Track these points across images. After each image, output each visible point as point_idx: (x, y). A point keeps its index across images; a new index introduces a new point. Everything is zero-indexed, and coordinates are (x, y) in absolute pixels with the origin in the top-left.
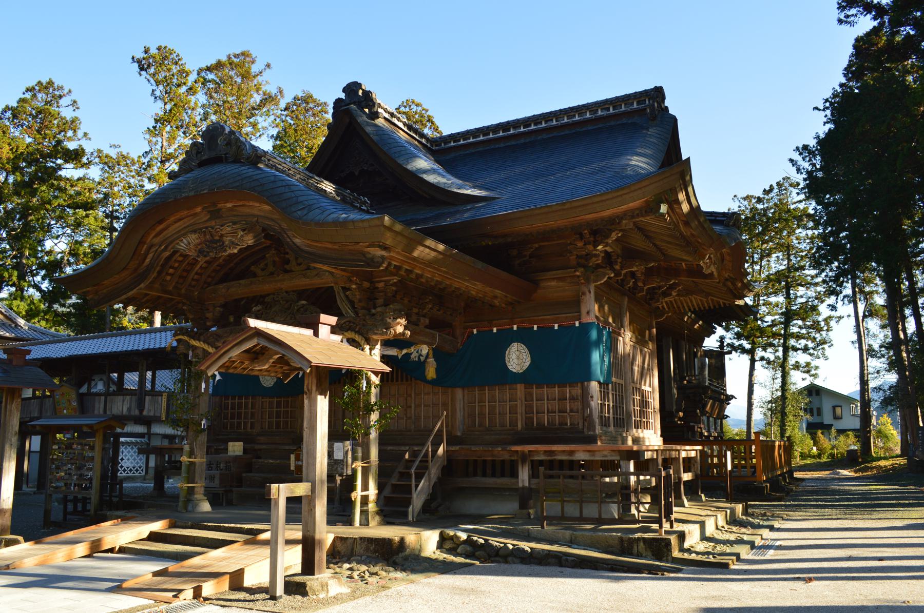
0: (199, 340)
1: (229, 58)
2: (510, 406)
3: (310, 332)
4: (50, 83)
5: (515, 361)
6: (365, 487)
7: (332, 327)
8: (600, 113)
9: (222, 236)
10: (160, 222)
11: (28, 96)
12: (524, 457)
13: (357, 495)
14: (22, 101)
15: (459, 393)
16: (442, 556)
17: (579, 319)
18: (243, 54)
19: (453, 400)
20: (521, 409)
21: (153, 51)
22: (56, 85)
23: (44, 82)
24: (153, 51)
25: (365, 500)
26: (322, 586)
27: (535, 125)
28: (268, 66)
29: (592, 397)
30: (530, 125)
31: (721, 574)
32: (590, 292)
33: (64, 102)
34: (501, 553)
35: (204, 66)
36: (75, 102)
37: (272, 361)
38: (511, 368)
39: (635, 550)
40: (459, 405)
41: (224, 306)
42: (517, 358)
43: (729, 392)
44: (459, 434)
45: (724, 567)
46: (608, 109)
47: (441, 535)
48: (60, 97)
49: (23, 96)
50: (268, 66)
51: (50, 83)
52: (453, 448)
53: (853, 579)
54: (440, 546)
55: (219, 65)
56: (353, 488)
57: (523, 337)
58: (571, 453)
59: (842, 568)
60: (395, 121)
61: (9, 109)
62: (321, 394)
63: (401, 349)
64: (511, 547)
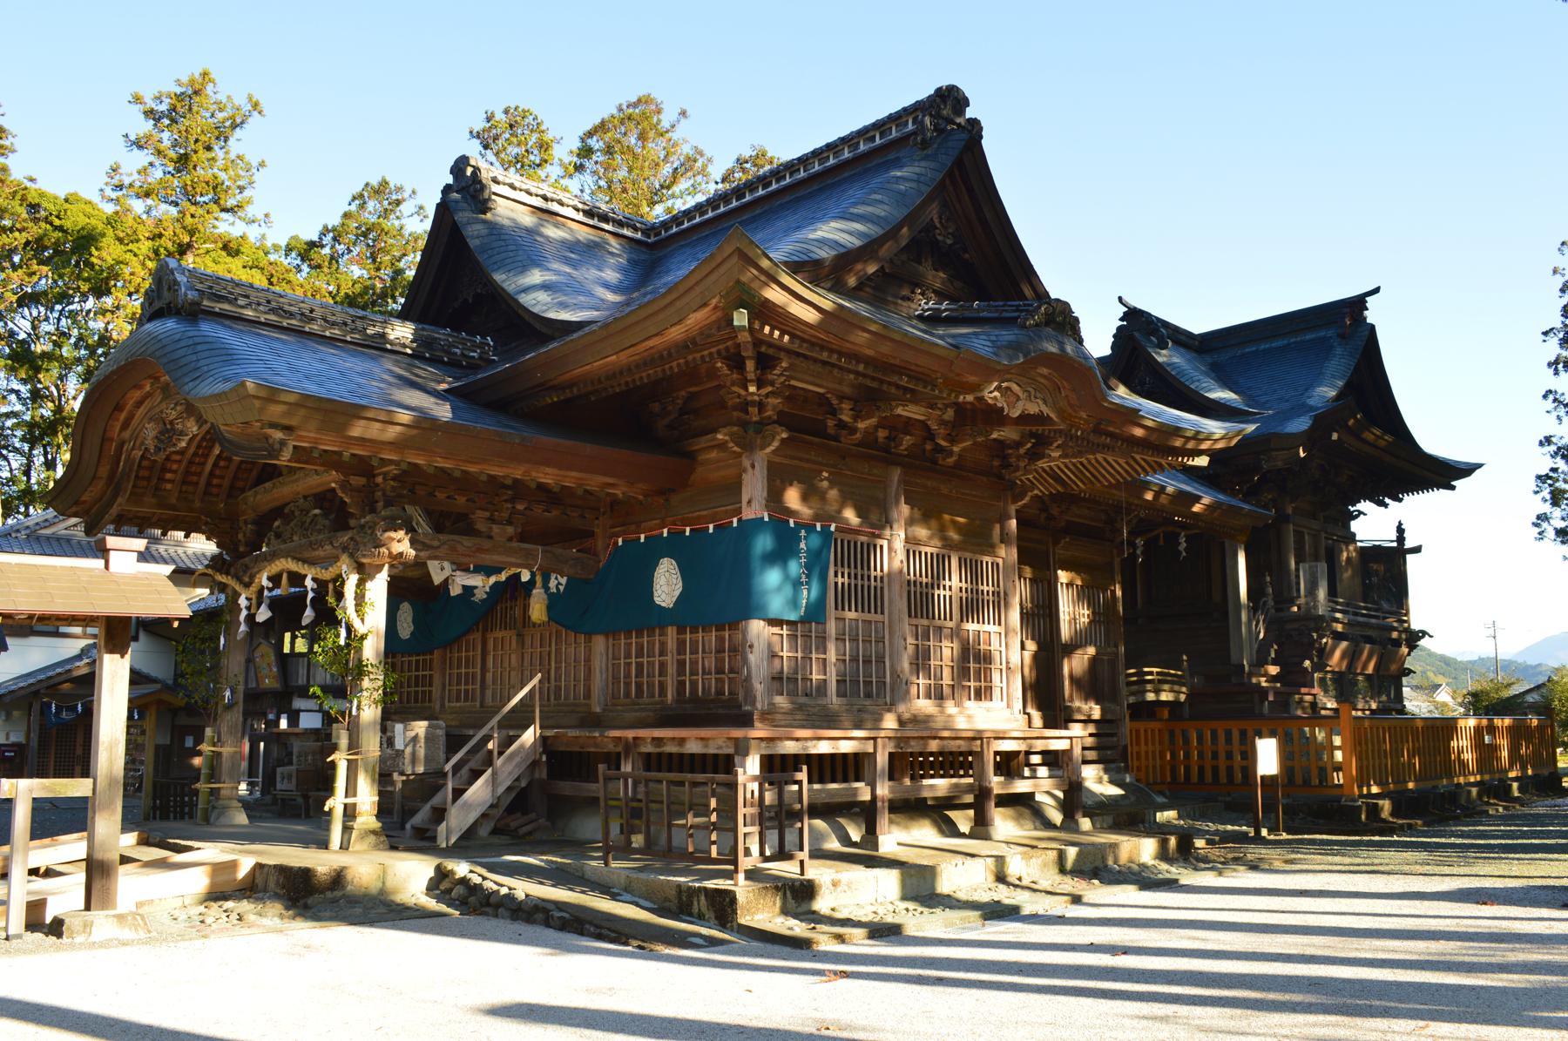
0: (227, 574)
1: (620, 109)
2: (669, 660)
3: (101, 563)
4: (384, 183)
5: (665, 588)
6: (351, 790)
7: (140, 553)
8: (862, 147)
9: (171, 423)
10: (119, 408)
11: (353, 207)
12: (630, 747)
13: (336, 803)
14: (346, 215)
15: (599, 643)
16: (432, 904)
17: (738, 512)
18: (639, 101)
19: (589, 651)
20: (672, 669)
21: (500, 116)
22: (392, 185)
23: (374, 182)
24: (500, 116)
25: (350, 813)
26: (85, 926)
27: (778, 181)
28: (683, 113)
29: (751, 646)
30: (770, 184)
31: (799, 960)
32: (753, 466)
33: (407, 208)
34: (492, 900)
35: (588, 127)
36: (421, 208)
37: (311, 595)
38: (657, 600)
39: (695, 910)
40: (599, 663)
41: (255, 523)
42: (667, 584)
43: (1415, 625)
44: (598, 710)
45: (799, 945)
46: (873, 139)
47: (438, 868)
48: (398, 203)
49: (347, 208)
50: (683, 113)
51: (384, 183)
52: (549, 733)
53: (940, 981)
54: (433, 887)
55: (601, 128)
56: (329, 790)
57: (675, 548)
58: (682, 741)
59: (855, 955)
60: (555, 207)
61: (328, 231)
62: (111, 652)
63: (488, 575)
64: (504, 891)
